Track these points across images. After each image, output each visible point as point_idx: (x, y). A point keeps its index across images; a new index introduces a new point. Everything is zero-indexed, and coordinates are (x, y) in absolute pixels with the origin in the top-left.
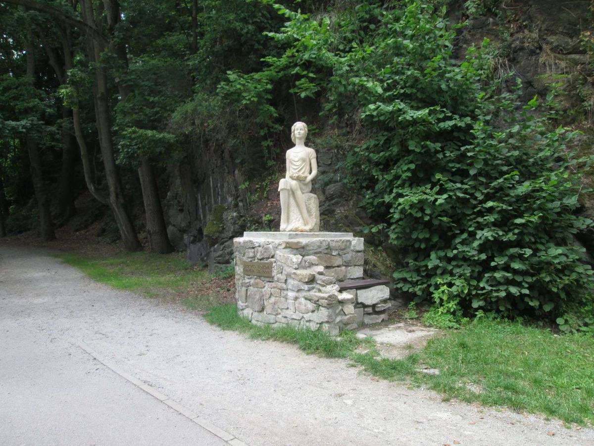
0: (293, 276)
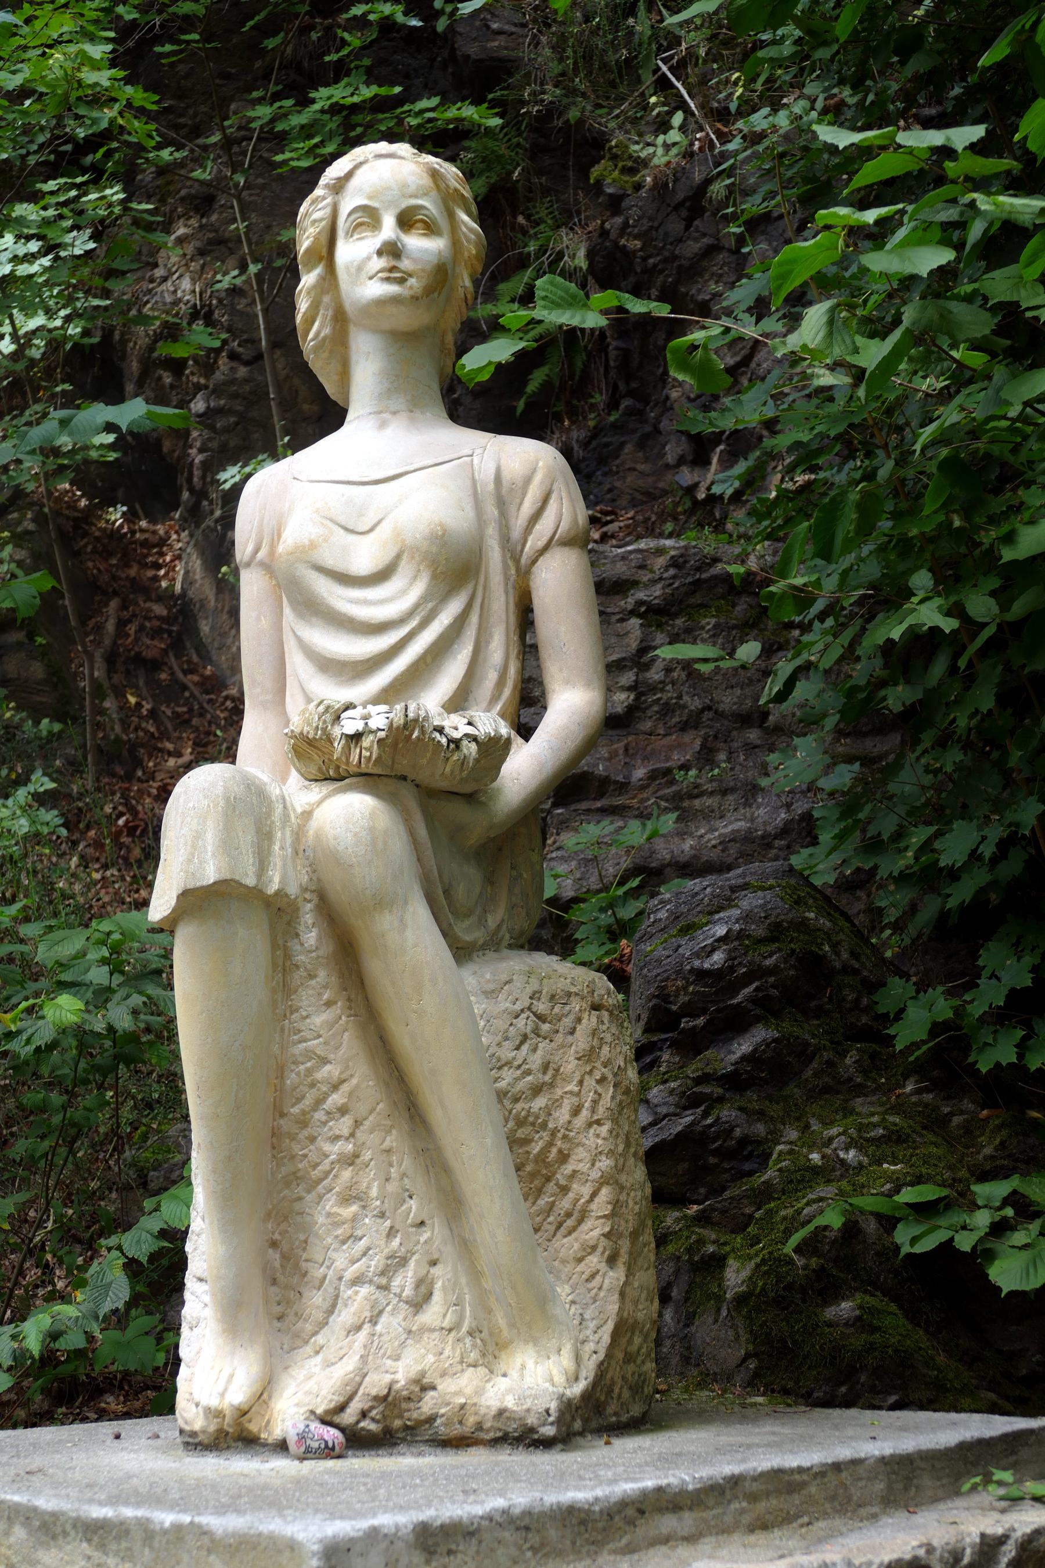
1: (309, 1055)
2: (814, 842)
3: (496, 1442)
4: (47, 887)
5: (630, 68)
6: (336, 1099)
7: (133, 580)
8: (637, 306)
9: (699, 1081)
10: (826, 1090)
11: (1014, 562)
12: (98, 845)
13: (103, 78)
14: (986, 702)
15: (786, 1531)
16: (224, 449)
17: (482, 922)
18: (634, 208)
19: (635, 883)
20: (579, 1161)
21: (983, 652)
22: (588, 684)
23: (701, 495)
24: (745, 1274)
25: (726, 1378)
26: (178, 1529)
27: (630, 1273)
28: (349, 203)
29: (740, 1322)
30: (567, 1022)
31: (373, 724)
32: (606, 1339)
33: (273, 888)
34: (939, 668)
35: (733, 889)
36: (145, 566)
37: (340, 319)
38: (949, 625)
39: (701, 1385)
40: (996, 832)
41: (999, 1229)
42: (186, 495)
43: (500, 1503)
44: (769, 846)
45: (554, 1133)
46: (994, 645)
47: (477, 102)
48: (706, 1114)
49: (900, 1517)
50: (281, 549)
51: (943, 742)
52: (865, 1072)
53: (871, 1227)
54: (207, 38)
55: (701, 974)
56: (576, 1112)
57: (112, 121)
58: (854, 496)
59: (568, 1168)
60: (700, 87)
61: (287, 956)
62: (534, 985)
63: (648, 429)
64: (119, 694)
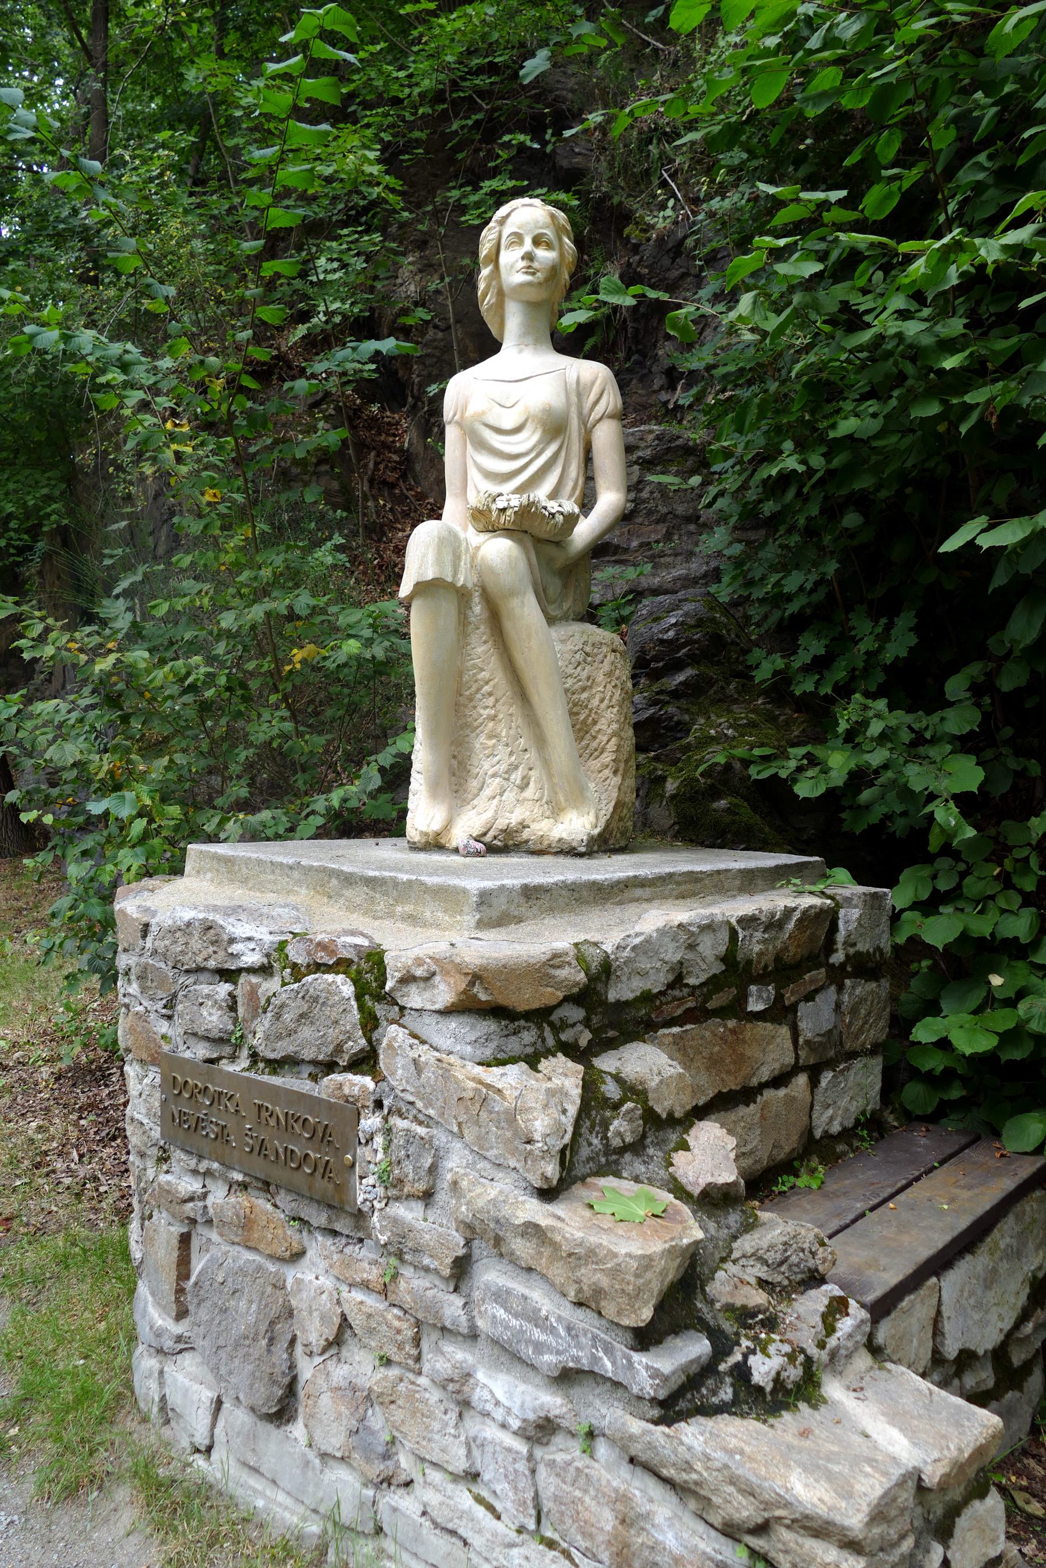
0: (522, 1247)
1: (475, 666)
2: (720, 581)
3: (556, 853)
4: (340, 592)
5: (647, 173)
6: (487, 688)
7: (383, 442)
8: (652, 294)
9: (658, 693)
10: (720, 700)
11: (835, 439)
12: (365, 573)
13: (375, 170)
14: (815, 511)
15: (693, 899)
16: (430, 375)
17: (560, 607)
18: (648, 251)
19: (631, 597)
20: (602, 724)
21: (813, 487)
22: (618, 490)
23: (671, 406)
24: (676, 785)
25: (663, 833)
26: (410, 881)
27: (623, 779)
28: (507, 230)
29: (672, 808)
30: (600, 657)
31: (512, 504)
32: (611, 809)
33: (460, 583)
34: (791, 494)
35: (680, 601)
36: (388, 435)
37: (501, 294)
38: (801, 468)
39: (651, 836)
40: (814, 577)
41: (800, 769)
42: (410, 399)
43: (562, 878)
44: (697, 583)
45: (591, 710)
46: (822, 481)
47: (567, 191)
48: (661, 709)
49: (747, 897)
50: (467, 414)
51: (790, 531)
52: (739, 693)
53: (737, 765)
54: (427, 152)
55: (662, 642)
56: (602, 701)
57: (379, 194)
58: (757, 401)
59: (597, 728)
60: (684, 185)
61: (466, 618)
62: (585, 638)
63: (645, 371)
64: (376, 500)
